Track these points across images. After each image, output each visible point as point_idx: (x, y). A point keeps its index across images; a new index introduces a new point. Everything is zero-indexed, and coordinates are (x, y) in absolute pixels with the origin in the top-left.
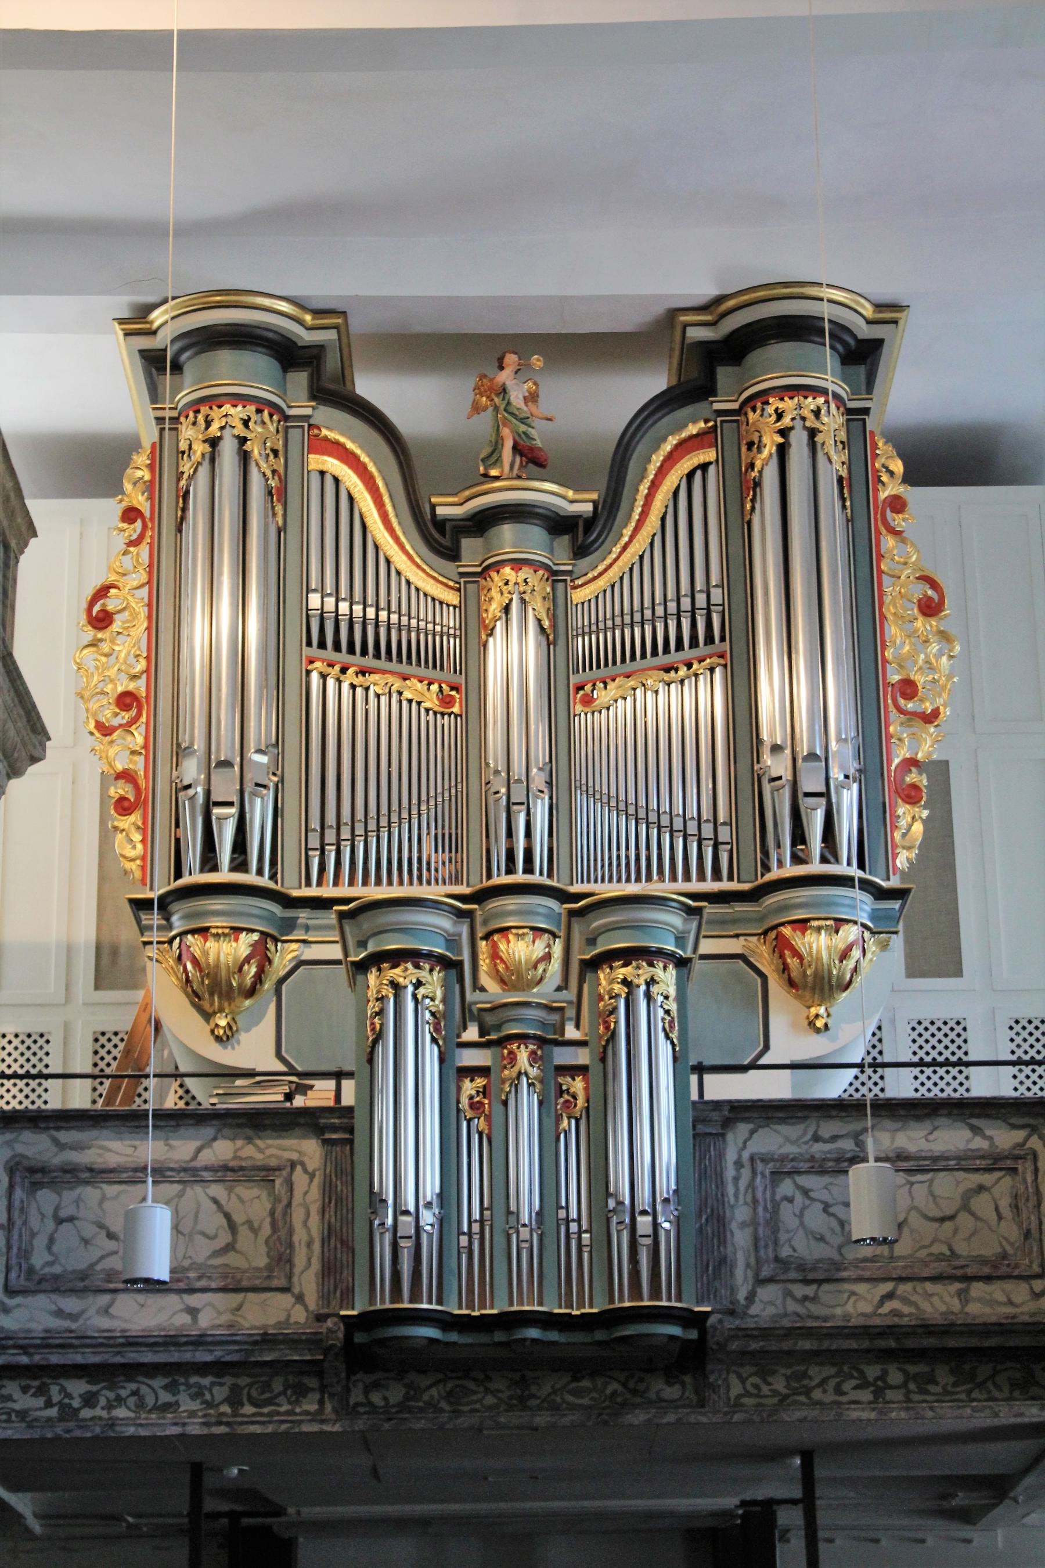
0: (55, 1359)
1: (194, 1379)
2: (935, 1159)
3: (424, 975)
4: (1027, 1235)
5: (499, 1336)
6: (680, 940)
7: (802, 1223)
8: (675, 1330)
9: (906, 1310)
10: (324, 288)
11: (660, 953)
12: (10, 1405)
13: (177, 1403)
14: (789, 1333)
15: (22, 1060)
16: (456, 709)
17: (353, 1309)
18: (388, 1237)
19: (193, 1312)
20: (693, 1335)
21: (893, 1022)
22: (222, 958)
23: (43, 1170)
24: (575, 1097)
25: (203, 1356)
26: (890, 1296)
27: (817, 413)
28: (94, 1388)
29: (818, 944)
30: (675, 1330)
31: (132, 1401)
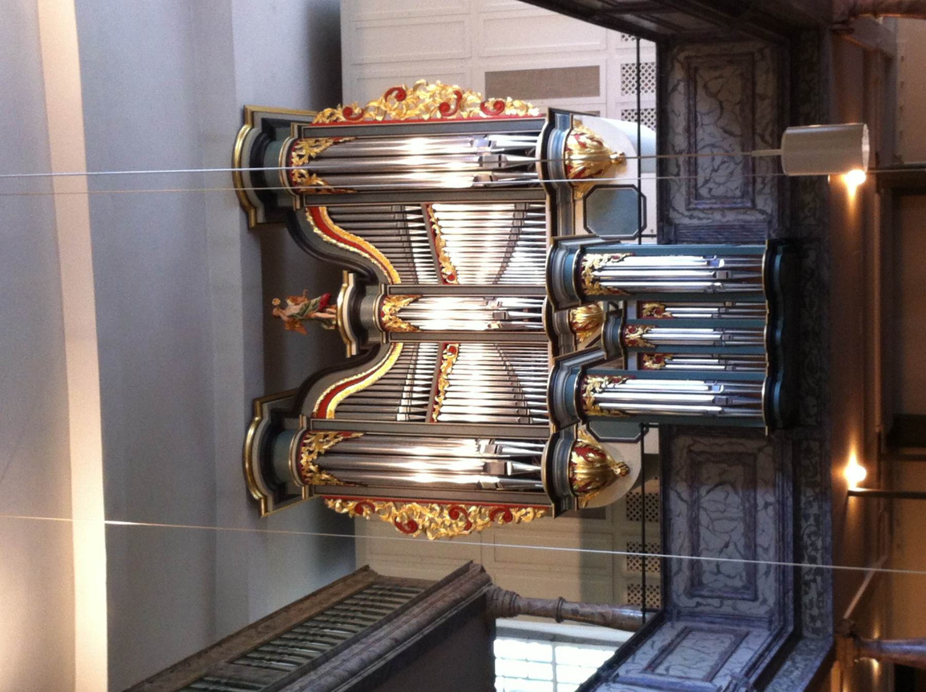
1: (802, 506)
3: (589, 387)
4: (731, 62)
6: (571, 251)
7: (724, 184)
8: (778, 260)
9: (770, 128)
10: (240, 410)
12: (815, 600)
13: (815, 515)
15: (636, 592)
16: (457, 345)
17: (764, 429)
18: (727, 410)
19: (767, 505)
20: (780, 248)
21: (623, 103)
22: (585, 471)
23: (692, 579)
24: (654, 308)
25: (790, 502)
27: (301, 156)
28: (806, 557)
29: (578, 160)
30: (778, 260)
31: (813, 538)
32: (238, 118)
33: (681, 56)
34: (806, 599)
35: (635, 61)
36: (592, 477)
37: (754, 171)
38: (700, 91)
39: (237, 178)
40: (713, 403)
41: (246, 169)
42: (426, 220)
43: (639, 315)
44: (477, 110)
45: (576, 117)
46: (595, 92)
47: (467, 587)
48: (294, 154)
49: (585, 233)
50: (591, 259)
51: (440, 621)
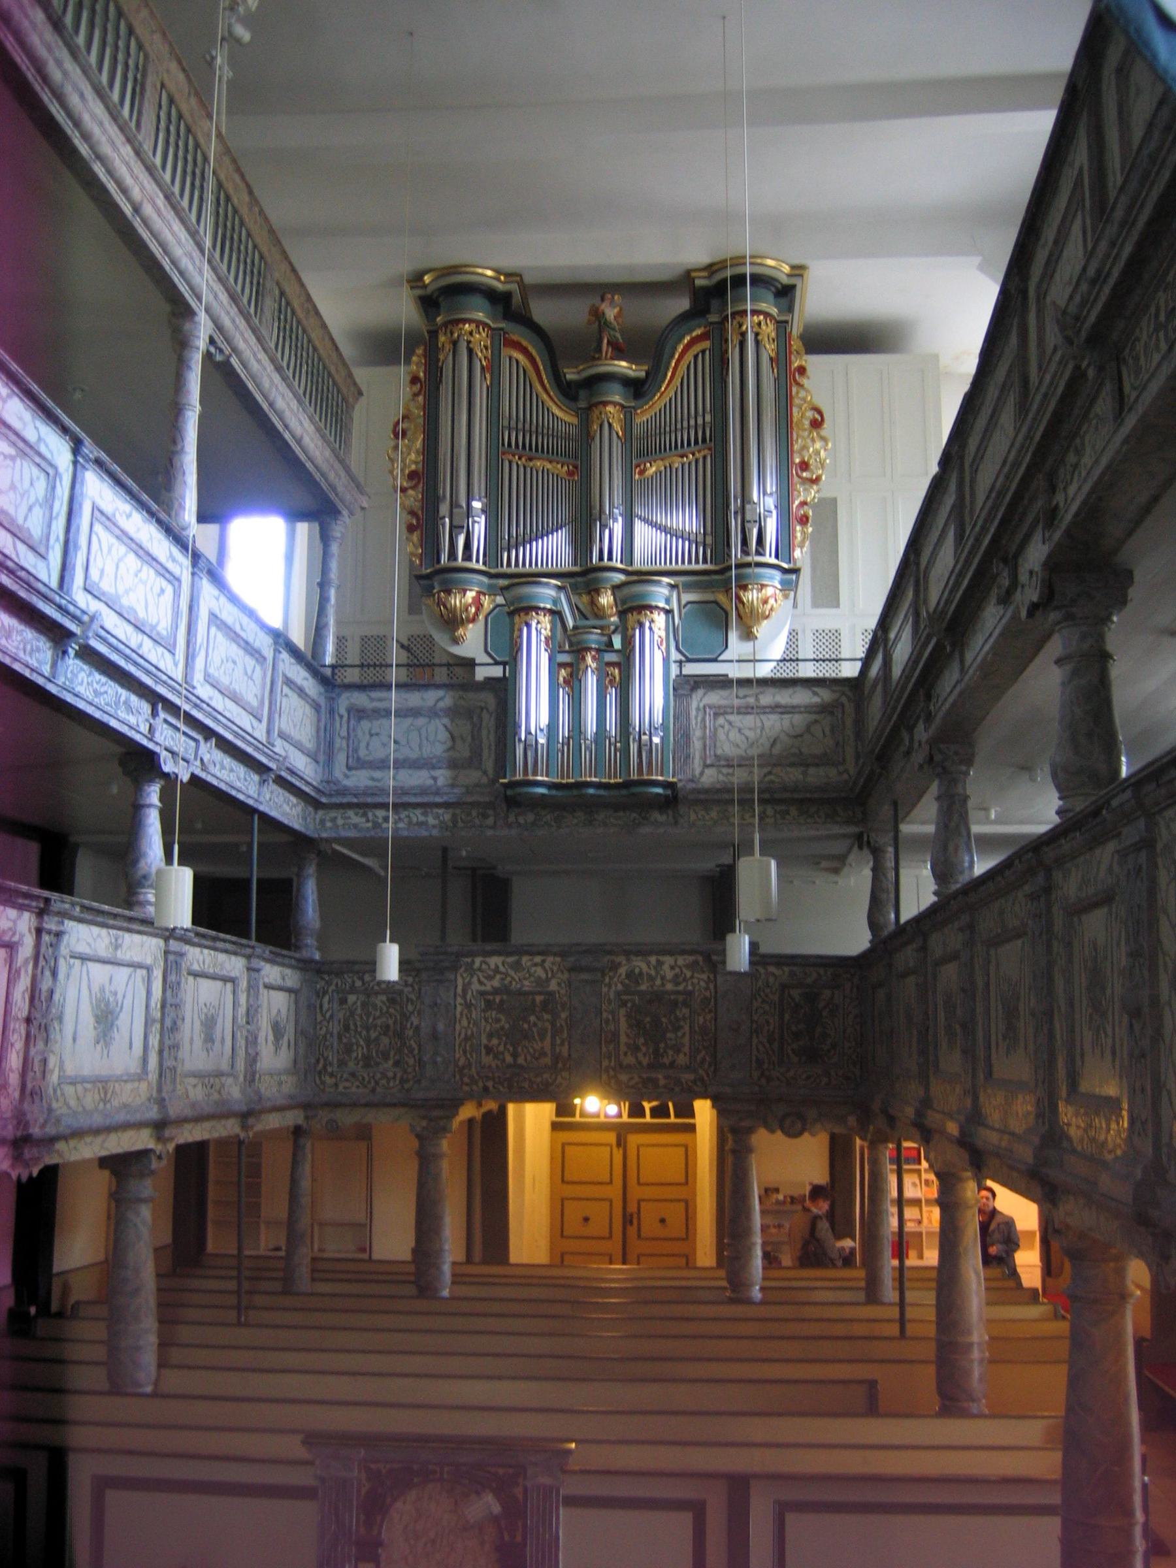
0: (369, 800)
2: (793, 707)
3: (541, 618)
4: (837, 744)
5: (575, 792)
6: (668, 601)
8: (659, 790)
10: (511, 262)
11: (657, 607)
14: (718, 791)
17: (505, 777)
18: (522, 746)
20: (669, 792)
21: (804, 631)
25: (438, 799)
26: (770, 773)
30: (659, 790)
31: (406, 820)
32: (796, 262)
33: (844, 699)
34: (350, 813)
35: (843, 656)
36: (453, 611)
37: (739, 766)
38: (814, 717)
39: (739, 260)
40: (528, 733)
41: (748, 270)
42: (697, 447)
43: (609, 664)
44: (802, 499)
45: (792, 594)
46: (816, 604)
47: (348, 497)
48: (761, 317)
49: (683, 602)
50: (660, 619)
51: (317, 476)
